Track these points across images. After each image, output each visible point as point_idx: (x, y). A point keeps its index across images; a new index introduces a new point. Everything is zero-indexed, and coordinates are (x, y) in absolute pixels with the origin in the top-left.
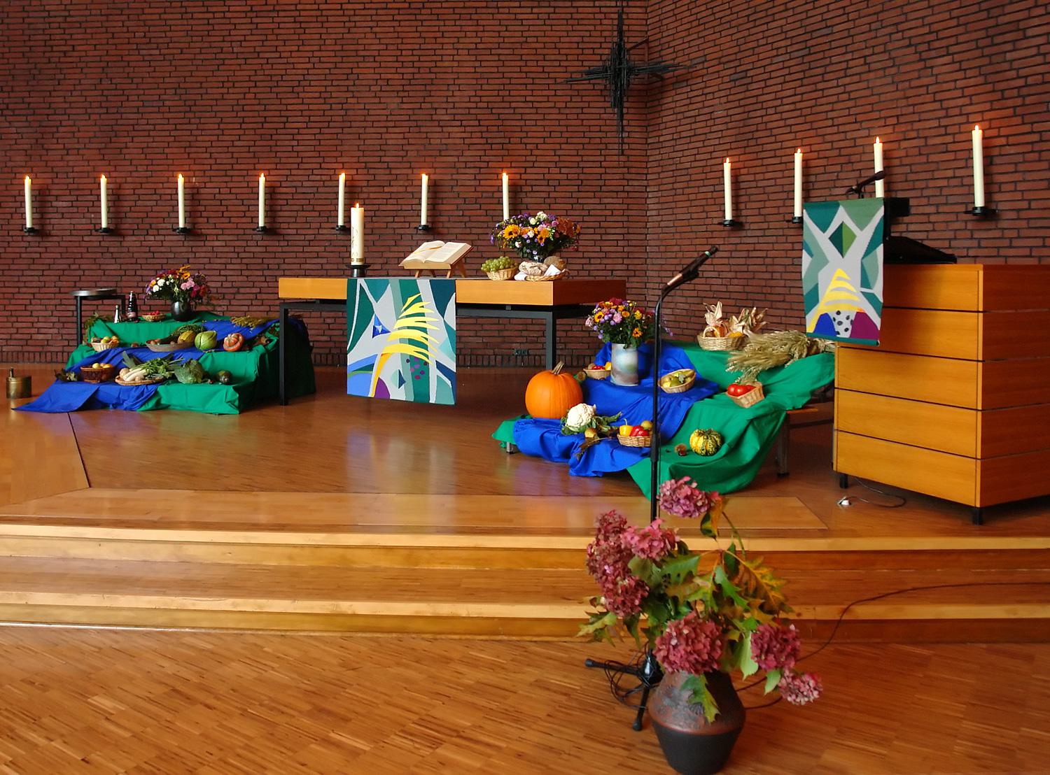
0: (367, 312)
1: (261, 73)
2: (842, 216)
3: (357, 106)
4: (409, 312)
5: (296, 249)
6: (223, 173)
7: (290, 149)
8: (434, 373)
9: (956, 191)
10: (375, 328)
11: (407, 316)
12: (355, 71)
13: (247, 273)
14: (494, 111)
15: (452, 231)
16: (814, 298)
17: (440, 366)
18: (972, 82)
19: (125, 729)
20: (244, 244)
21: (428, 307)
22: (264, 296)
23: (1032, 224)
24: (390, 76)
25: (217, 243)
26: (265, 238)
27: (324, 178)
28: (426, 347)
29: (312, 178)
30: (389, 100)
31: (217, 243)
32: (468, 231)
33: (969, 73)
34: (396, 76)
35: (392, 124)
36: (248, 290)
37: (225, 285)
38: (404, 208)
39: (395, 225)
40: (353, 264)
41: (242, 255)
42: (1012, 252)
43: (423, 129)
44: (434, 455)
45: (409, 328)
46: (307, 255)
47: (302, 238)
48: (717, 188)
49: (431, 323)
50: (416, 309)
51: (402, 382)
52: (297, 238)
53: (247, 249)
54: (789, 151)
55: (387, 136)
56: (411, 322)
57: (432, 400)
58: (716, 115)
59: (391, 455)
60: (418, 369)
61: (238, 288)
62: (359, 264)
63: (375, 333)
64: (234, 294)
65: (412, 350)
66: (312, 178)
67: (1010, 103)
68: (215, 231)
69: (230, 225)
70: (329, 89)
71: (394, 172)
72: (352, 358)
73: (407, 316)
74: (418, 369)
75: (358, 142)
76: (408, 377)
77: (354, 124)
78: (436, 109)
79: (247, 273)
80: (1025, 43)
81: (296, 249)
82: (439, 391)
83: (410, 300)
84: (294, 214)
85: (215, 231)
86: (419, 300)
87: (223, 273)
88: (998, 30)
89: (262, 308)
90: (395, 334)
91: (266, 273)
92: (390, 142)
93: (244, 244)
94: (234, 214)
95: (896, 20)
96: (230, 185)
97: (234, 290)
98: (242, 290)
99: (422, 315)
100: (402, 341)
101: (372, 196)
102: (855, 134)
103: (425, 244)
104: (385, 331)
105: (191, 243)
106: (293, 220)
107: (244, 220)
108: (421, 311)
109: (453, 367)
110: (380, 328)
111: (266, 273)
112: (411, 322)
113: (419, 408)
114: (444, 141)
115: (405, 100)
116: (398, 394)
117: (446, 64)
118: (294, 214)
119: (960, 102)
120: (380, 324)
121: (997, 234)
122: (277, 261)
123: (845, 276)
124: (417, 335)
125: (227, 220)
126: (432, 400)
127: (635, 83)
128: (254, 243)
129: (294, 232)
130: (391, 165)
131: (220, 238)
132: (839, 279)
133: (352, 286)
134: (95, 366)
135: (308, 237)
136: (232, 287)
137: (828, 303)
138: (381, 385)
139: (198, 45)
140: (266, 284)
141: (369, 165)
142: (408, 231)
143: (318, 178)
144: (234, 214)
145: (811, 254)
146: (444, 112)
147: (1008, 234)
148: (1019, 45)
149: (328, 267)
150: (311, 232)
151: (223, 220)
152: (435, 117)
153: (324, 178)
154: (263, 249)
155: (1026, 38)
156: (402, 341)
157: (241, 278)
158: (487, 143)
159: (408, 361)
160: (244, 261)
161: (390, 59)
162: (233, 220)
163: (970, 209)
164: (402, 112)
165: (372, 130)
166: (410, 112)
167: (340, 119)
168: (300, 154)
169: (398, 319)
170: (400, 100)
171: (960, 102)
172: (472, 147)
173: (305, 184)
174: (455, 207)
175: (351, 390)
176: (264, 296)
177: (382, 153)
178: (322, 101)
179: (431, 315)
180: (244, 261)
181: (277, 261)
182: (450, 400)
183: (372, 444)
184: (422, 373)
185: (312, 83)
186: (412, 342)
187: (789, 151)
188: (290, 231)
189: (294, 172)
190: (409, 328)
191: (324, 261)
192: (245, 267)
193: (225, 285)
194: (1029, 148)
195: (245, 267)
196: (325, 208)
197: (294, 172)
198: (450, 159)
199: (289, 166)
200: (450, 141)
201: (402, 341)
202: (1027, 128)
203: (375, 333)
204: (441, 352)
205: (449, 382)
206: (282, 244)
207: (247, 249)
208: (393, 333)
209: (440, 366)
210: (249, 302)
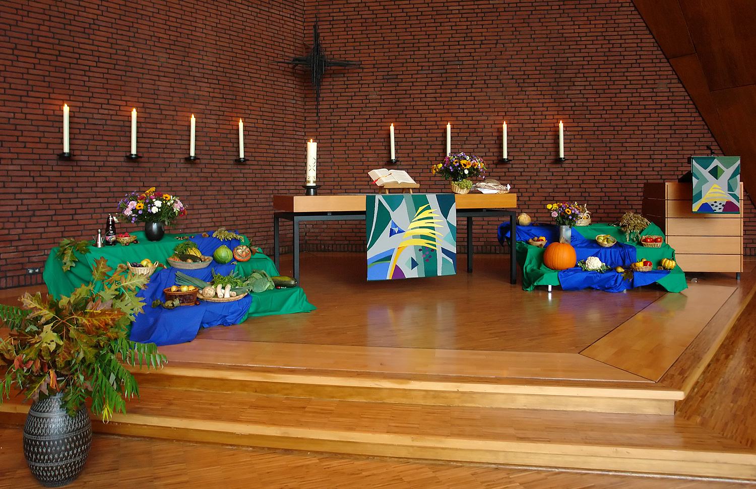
0: (385, 218)
1: (56, 8)
2: (716, 163)
3: (137, 55)
4: (421, 216)
5: (88, 174)
6: (18, 98)
7: (82, 83)
8: (440, 256)
9: (539, 150)
10: (392, 230)
11: (419, 220)
12: (586, 63)
13: (43, 196)
14: (227, 75)
15: (203, 161)
16: (700, 196)
17: (444, 251)
18: (548, 101)
20: (40, 168)
21: (435, 212)
22: (59, 218)
23: (579, 165)
24: (161, 35)
25: (11, 168)
26: (59, 163)
27: (111, 112)
28: (434, 240)
29: (101, 111)
30: (160, 54)
31: (11, 168)
32: (212, 161)
33: (546, 97)
34: (165, 36)
35: (162, 74)
36: (44, 213)
37: (20, 208)
38: (172, 142)
39: (165, 156)
40: (308, 185)
41: (37, 179)
42: (569, 178)
43: (183, 81)
44: (440, 310)
45: (420, 227)
46: (97, 179)
47: (93, 164)
49: (437, 223)
50: (426, 214)
51: (414, 264)
52: (89, 164)
53: (42, 173)
54: (387, 124)
55: (159, 83)
56: (423, 223)
57: (439, 274)
58: (370, 97)
59: (406, 318)
60: (429, 254)
61: (34, 211)
62: (314, 185)
63: (392, 233)
64: (30, 216)
65: (423, 243)
66: (101, 111)
67: (567, 112)
68: (10, 156)
69: (25, 150)
70: (114, 36)
71: (164, 112)
72: (371, 254)
73: (419, 220)
74: (429, 254)
75: (137, 85)
77: (134, 69)
78: (192, 67)
79: (43, 196)
80: (574, 88)
81: (88, 174)
82: (444, 267)
83: (421, 209)
84: (86, 142)
85: (10, 156)
86: (429, 208)
87: (18, 196)
88: (560, 80)
89: (58, 229)
90: (409, 233)
91: (61, 195)
92: (161, 88)
93: (40, 168)
94: (30, 139)
95: (505, 65)
96: (25, 111)
97: (30, 213)
98: (37, 213)
99: (432, 218)
100: (414, 235)
101: (148, 131)
102: (479, 118)
103: (404, 173)
104: (400, 231)
106: (85, 147)
107: (39, 146)
108: (431, 215)
109: (454, 250)
110: (396, 230)
111: (61, 195)
112: (423, 223)
113: (429, 282)
114: (197, 93)
115: (171, 56)
116: (411, 273)
117: (198, 34)
118: (86, 142)
119: (542, 109)
120: (396, 226)
121: (562, 170)
122: (70, 185)
123: (718, 187)
124: (426, 232)
125: (23, 145)
126: (439, 274)
127: (312, 70)
128: (50, 168)
129: (86, 158)
130: (162, 107)
131: (15, 162)
132: (715, 188)
133: (370, 202)
134: (293, 283)
135: (98, 164)
136: (28, 210)
137: (707, 199)
138: (397, 270)
140: (60, 207)
141: (146, 105)
142: (174, 160)
143: (106, 112)
144: (30, 139)
145: (698, 179)
146: (197, 70)
147: (567, 170)
148: (571, 88)
149: (115, 189)
150: (100, 159)
151: (19, 144)
152: (191, 73)
153: (111, 112)
154: (58, 174)
155: (574, 85)
156: (414, 237)
157: (36, 201)
158: (223, 98)
159: (420, 250)
160: (40, 185)
161: (161, 21)
162: (28, 145)
163: (128, 154)
164: (170, 66)
165: (148, 77)
166: (175, 67)
167: (124, 63)
168: (91, 90)
169: (411, 222)
170: (167, 56)
171: (542, 109)
172: (215, 99)
173: (95, 116)
174: (204, 143)
175: (371, 277)
176: (59, 218)
177: (155, 97)
178: (109, 45)
179: (437, 218)
180: (40, 185)
181: (70, 185)
182: (453, 272)
183: (390, 313)
184: (430, 257)
185: (101, 28)
186: (423, 237)
187: (387, 124)
188: (82, 158)
189: (86, 105)
190: (420, 227)
191: (112, 184)
192: (40, 190)
193: (20, 208)
194: (577, 133)
195: (40, 190)
196: (112, 139)
197: (86, 105)
198: (200, 106)
199: (81, 99)
200: (201, 93)
201: (414, 235)
202: (576, 124)
203: (392, 233)
204: (445, 241)
205: (451, 261)
206: (75, 169)
207: (42, 173)
208: (407, 232)
209: (444, 251)
210: (45, 224)
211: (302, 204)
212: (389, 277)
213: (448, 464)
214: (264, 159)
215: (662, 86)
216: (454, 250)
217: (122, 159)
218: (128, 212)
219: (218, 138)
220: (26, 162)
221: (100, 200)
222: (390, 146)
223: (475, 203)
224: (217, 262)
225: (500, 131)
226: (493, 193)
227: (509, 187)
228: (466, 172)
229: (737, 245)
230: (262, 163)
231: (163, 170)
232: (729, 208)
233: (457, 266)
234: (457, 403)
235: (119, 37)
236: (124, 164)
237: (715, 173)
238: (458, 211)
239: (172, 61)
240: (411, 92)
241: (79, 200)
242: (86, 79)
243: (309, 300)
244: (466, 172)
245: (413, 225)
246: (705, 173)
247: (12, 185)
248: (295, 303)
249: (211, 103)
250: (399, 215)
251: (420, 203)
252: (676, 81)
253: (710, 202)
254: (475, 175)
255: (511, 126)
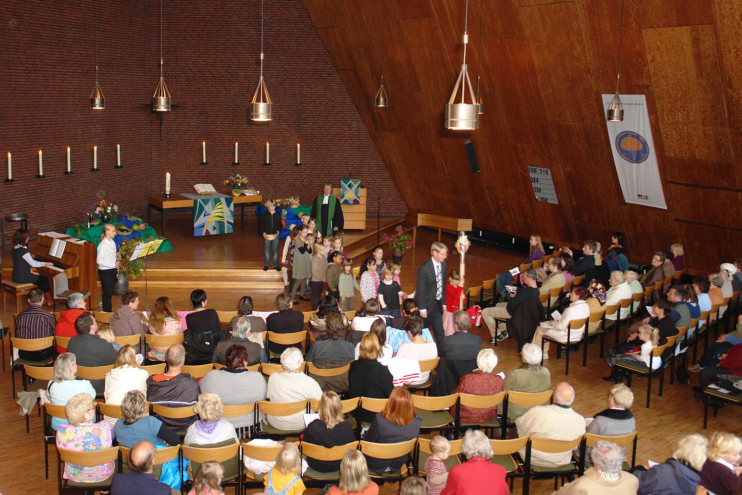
0: (202, 209)
2: (350, 182)
8: (226, 224)
17: (228, 222)
19: (127, 447)
25: (17, 185)
44: (226, 249)
48: (45, 170)
51: (215, 228)
56: (218, 211)
57: (226, 232)
60: (221, 224)
63: (205, 215)
65: (219, 219)
72: (195, 225)
74: (221, 224)
76: (217, 227)
82: (228, 229)
86: (221, 204)
90: (212, 215)
93: (28, 183)
100: (216, 215)
104: (208, 215)
105: (7, 186)
109: (232, 222)
112: (218, 211)
113: (221, 236)
115: (83, 114)
116: (213, 232)
126: (226, 232)
139: (6, 86)
183: (204, 250)
186: (218, 216)
191: (58, 188)
201: (216, 215)
203: (205, 215)
204: (228, 218)
209: (228, 222)
211: (167, 205)
212: (204, 234)
213: (221, 289)
214: (129, 163)
215: (355, 124)
216: (232, 222)
217: (62, 174)
218: (97, 212)
219: (108, 155)
220: (23, 181)
221: (53, 196)
222: (202, 153)
223: (243, 200)
224: (134, 232)
225: (265, 146)
226: (251, 194)
227: (259, 192)
228: (239, 185)
229: (363, 217)
230: (128, 166)
231: (80, 177)
232: (356, 202)
233: (233, 228)
234: (225, 275)
235: (59, 109)
236: (63, 176)
237: (350, 186)
238: (235, 205)
239: (83, 116)
240: (215, 122)
241: (44, 198)
242: (45, 134)
243: (172, 245)
244: (239, 185)
245: (214, 212)
246: (346, 186)
247: (18, 193)
248: (166, 247)
249: (102, 136)
250: (208, 208)
251: (217, 201)
252: (361, 122)
253: (348, 199)
254: (244, 186)
255: (271, 144)
